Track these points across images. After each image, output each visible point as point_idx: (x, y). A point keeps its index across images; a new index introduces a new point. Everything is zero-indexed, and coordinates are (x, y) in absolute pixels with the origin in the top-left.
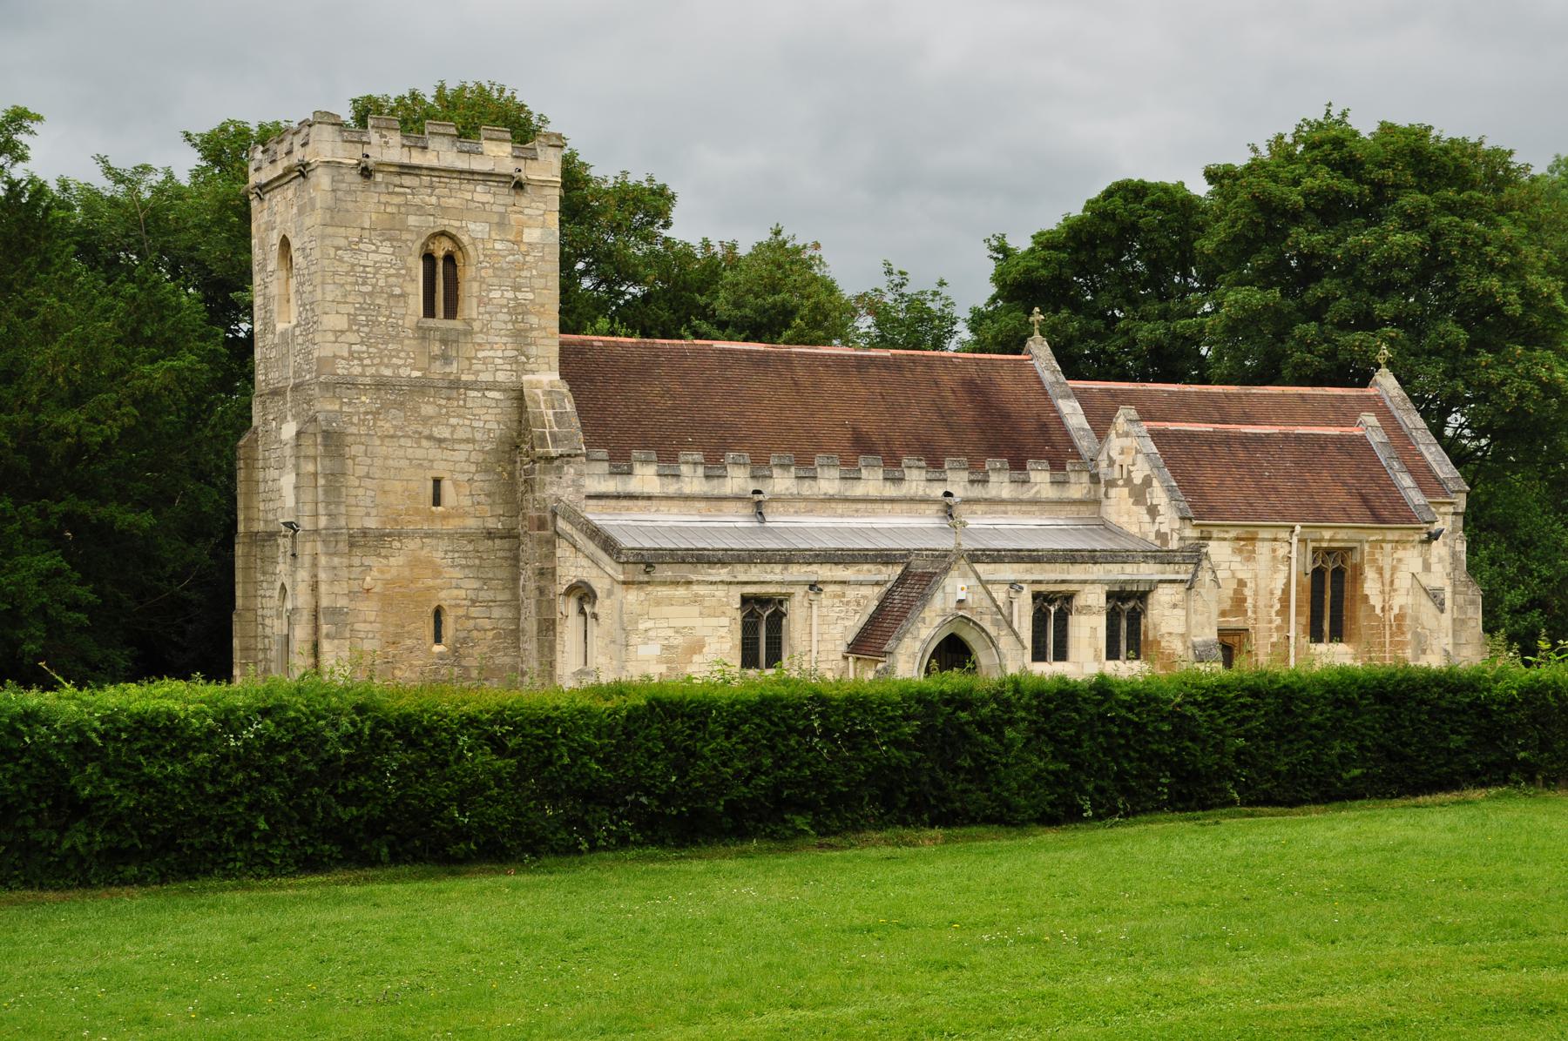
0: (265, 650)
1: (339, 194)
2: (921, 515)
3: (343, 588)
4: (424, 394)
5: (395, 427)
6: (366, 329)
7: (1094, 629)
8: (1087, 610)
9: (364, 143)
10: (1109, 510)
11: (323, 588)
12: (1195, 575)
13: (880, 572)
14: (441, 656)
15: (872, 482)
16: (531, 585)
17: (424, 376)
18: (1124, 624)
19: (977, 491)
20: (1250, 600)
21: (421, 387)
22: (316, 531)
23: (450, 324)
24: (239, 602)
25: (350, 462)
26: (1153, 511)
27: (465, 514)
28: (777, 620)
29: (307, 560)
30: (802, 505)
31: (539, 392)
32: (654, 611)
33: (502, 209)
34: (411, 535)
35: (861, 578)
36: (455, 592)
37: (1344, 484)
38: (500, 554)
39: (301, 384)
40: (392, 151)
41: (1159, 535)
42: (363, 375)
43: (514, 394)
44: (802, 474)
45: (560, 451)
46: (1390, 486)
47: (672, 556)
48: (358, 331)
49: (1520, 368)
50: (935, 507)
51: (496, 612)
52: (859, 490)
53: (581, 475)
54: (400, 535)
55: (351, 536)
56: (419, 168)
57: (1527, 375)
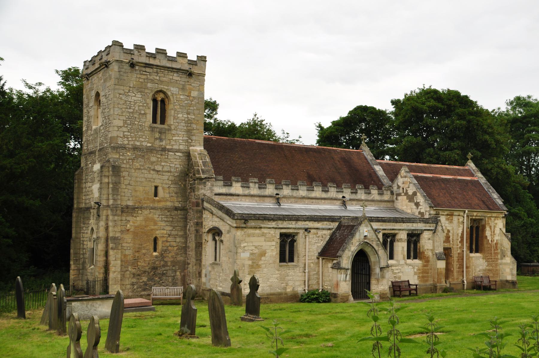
0: (83, 254)
1: (121, 73)
2: (335, 205)
3: (119, 229)
4: (152, 152)
5: (140, 165)
6: (130, 126)
7: (403, 248)
8: (401, 240)
9: (132, 54)
10: (398, 204)
11: (110, 229)
12: (436, 228)
13: (330, 225)
14: (156, 257)
15: (318, 192)
16: (193, 229)
17: (152, 146)
18: (412, 246)
19: (353, 196)
20: (451, 237)
21: (151, 150)
22: (108, 206)
23: (162, 126)
24: (74, 235)
25: (122, 179)
26: (417, 205)
27: (167, 201)
28: (293, 241)
29: (104, 218)
30: (293, 200)
31: (196, 153)
32: (247, 239)
33: (183, 83)
34: (146, 208)
35: (324, 227)
36: (162, 231)
37: (476, 197)
38: (180, 216)
39: (103, 148)
40: (142, 58)
41: (420, 213)
42: (128, 144)
43: (186, 154)
44: (293, 188)
45: (205, 176)
46: (490, 198)
47: (254, 217)
48: (127, 127)
49: (496, 164)
50: (339, 202)
51: (178, 240)
52: (313, 194)
53: (213, 185)
54: (141, 208)
55: (122, 208)
56: (153, 65)
57: (498, 167)
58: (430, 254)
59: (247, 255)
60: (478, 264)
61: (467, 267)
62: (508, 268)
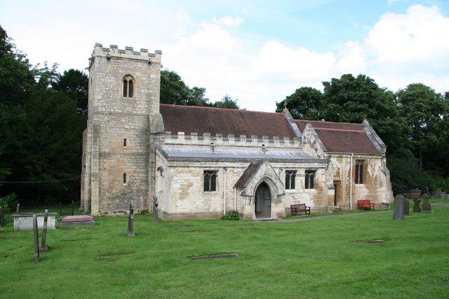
8: (300, 175)
19: (270, 145)
28: (214, 177)
32: (178, 175)
51: (141, 175)
58: (323, 185)
59: (178, 186)
60: (362, 192)
61: (353, 194)
62: (384, 194)
